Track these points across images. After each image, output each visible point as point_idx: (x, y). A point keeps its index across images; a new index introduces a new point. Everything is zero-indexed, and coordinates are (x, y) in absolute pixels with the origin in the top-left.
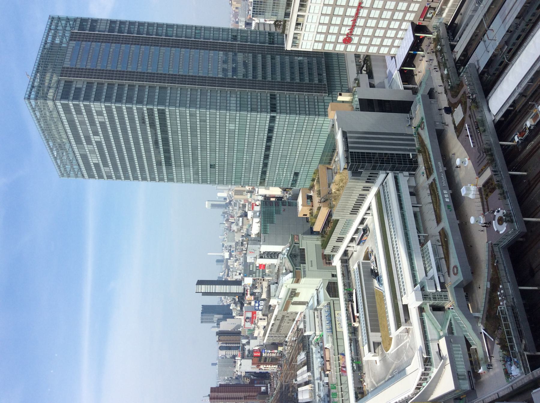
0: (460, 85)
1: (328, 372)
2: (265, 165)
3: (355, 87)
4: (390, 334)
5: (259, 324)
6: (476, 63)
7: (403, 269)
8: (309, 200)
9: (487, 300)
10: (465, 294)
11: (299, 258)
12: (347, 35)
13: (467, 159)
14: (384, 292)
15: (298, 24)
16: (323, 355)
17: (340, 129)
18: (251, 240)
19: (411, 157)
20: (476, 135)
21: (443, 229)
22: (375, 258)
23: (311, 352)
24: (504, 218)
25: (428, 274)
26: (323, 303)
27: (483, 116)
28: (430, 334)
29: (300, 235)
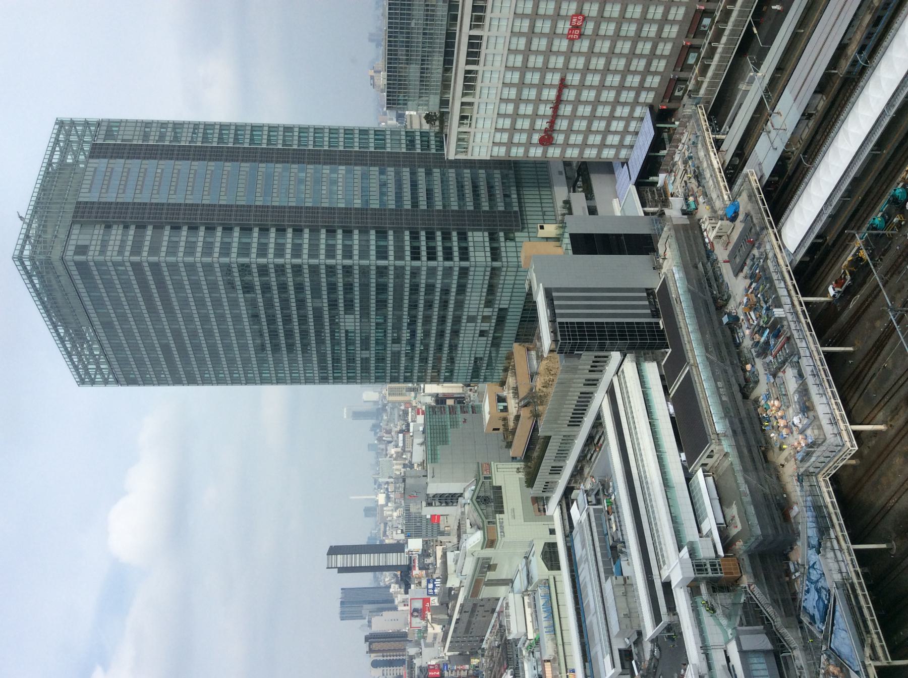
12: (546, 131)
15: (463, 118)
23: (520, 668)
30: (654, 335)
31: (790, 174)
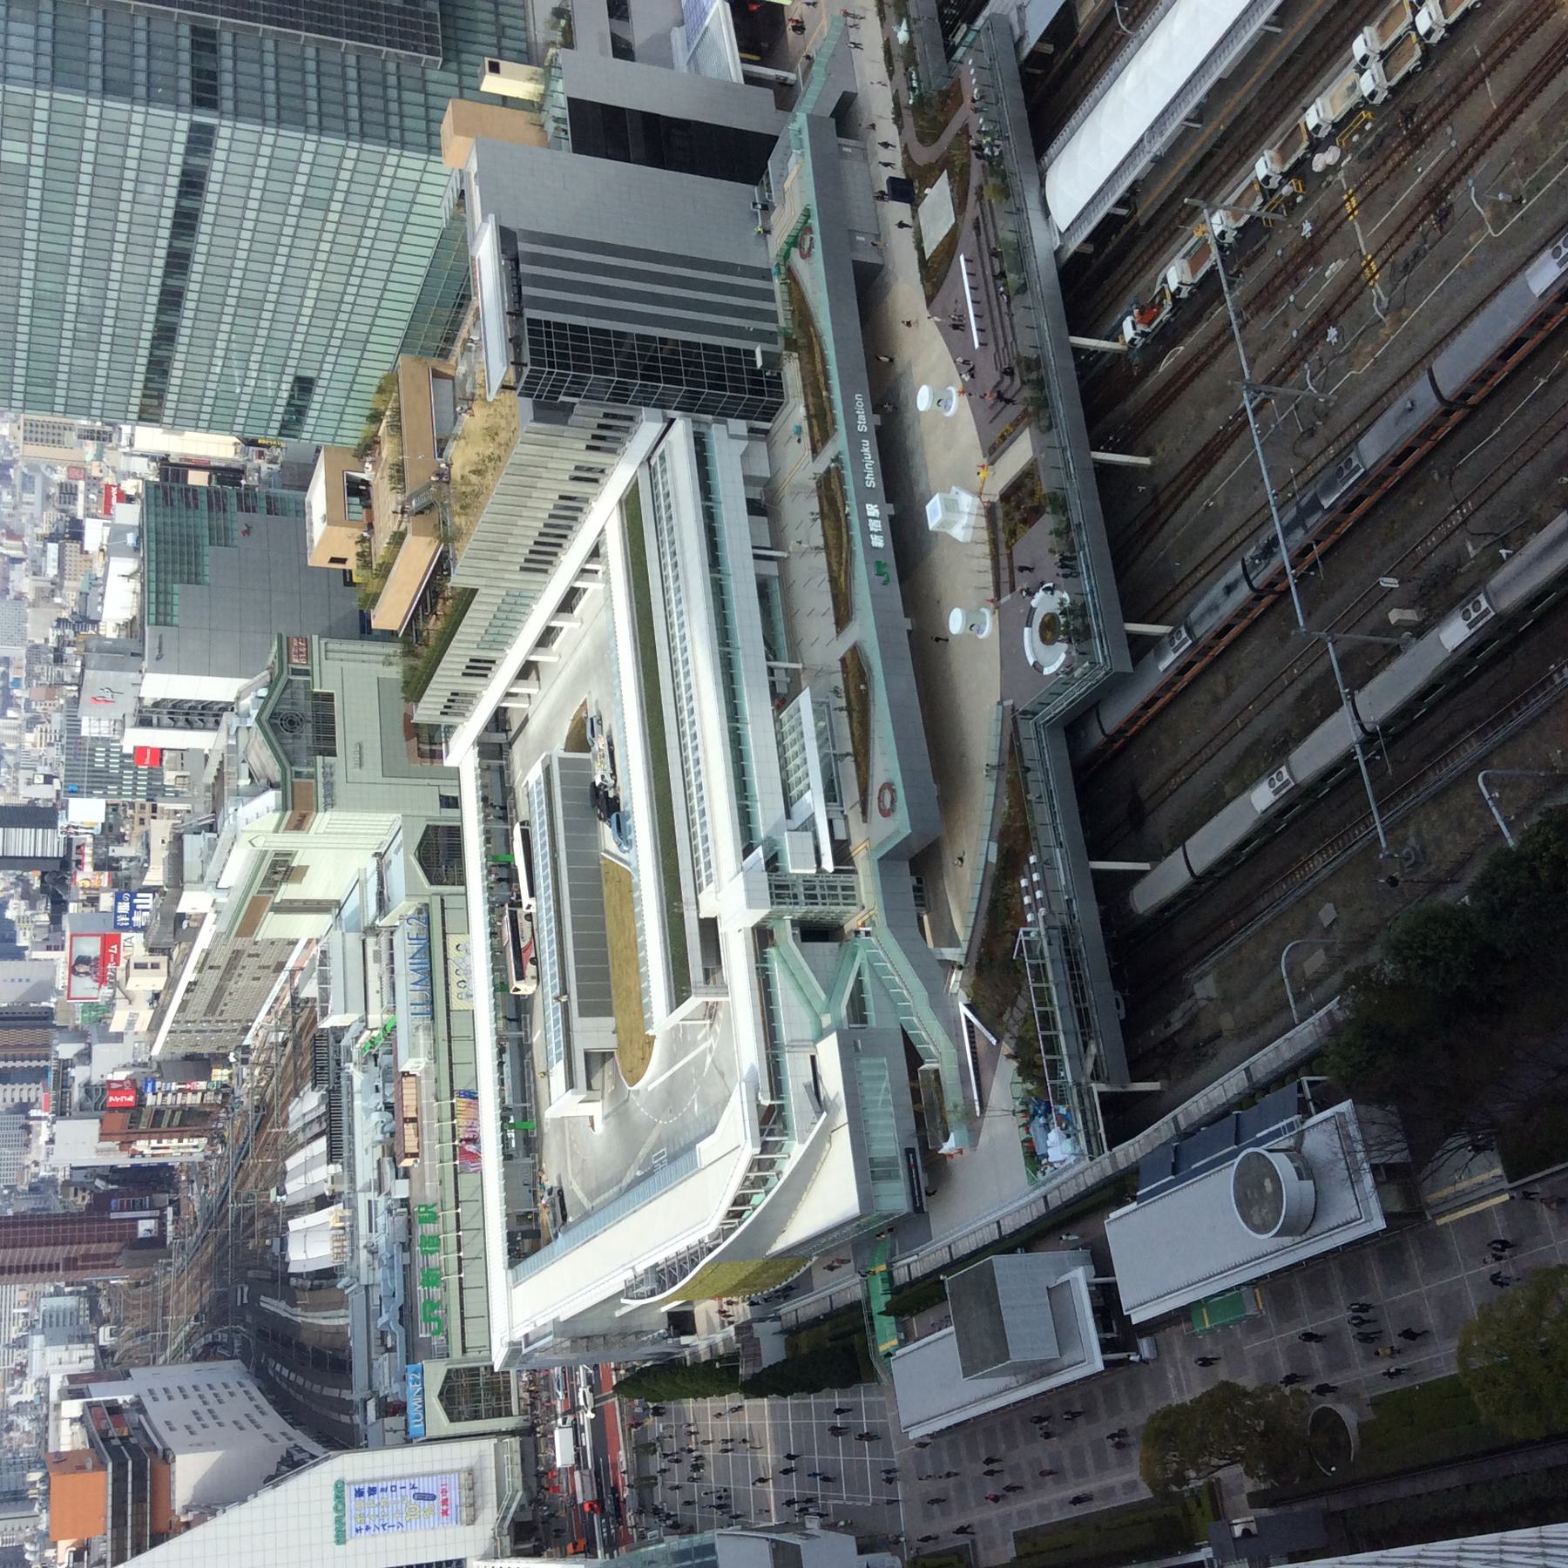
0: (951, 97)
1: (408, 1162)
2: (165, 335)
3: (553, 44)
4: (650, 1023)
5: (131, 986)
6: (1014, 17)
7: (709, 791)
8: (356, 500)
9: (985, 905)
10: (912, 881)
11: (307, 731)
13: (953, 390)
14: (637, 870)
16: (391, 1100)
17: (491, 217)
18: (100, 650)
19: (759, 363)
20: (994, 303)
21: (855, 650)
22: (610, 744)
23: (344, 1090)
24: (1062, 620)
25: (795, 809)
26: (403, 905)
27: (1022, 230)
28: (789, 1023)
29: (315, 638)
30: (687, 364)
31: (1082, 45)
